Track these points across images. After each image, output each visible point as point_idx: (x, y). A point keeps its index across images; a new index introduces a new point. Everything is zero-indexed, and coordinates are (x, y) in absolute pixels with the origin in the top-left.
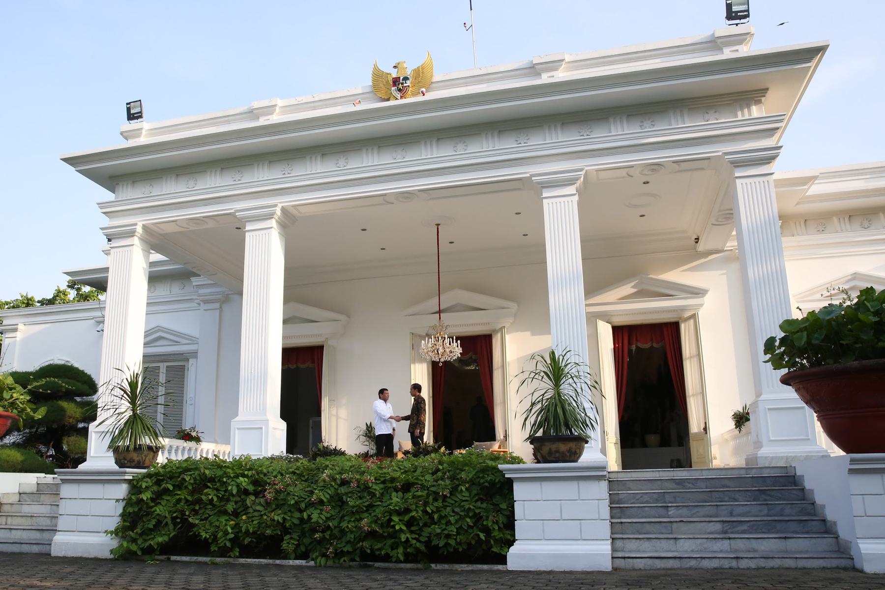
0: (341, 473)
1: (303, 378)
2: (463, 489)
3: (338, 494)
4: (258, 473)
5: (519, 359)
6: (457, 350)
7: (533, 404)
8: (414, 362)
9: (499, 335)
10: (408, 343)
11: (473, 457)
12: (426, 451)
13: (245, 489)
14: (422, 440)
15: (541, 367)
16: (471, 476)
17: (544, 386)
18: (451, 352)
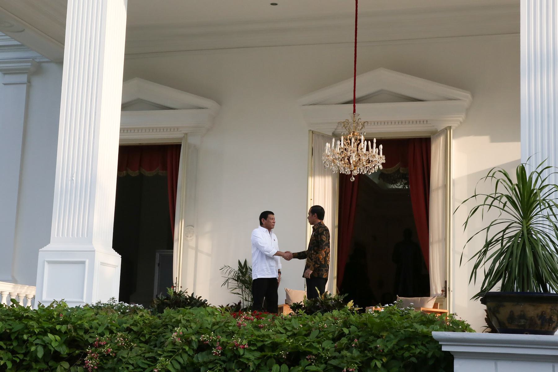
0: (198, 333)
1: (149, 187)
2: (379, 364)
3: (193, 364)
4: (75, 330)
5: (470, 177)
6: (378, 159)
7: (488, 244)
8: (313, 175)
9: (442, 139)
10: (305, 144)
11: (395, 318)
12: (326, 307)
13: (56, 352)
14: (322, 289)
15: (503, 190)
16: (390, 346)
17: (506, 219)
18: (369, 161)
